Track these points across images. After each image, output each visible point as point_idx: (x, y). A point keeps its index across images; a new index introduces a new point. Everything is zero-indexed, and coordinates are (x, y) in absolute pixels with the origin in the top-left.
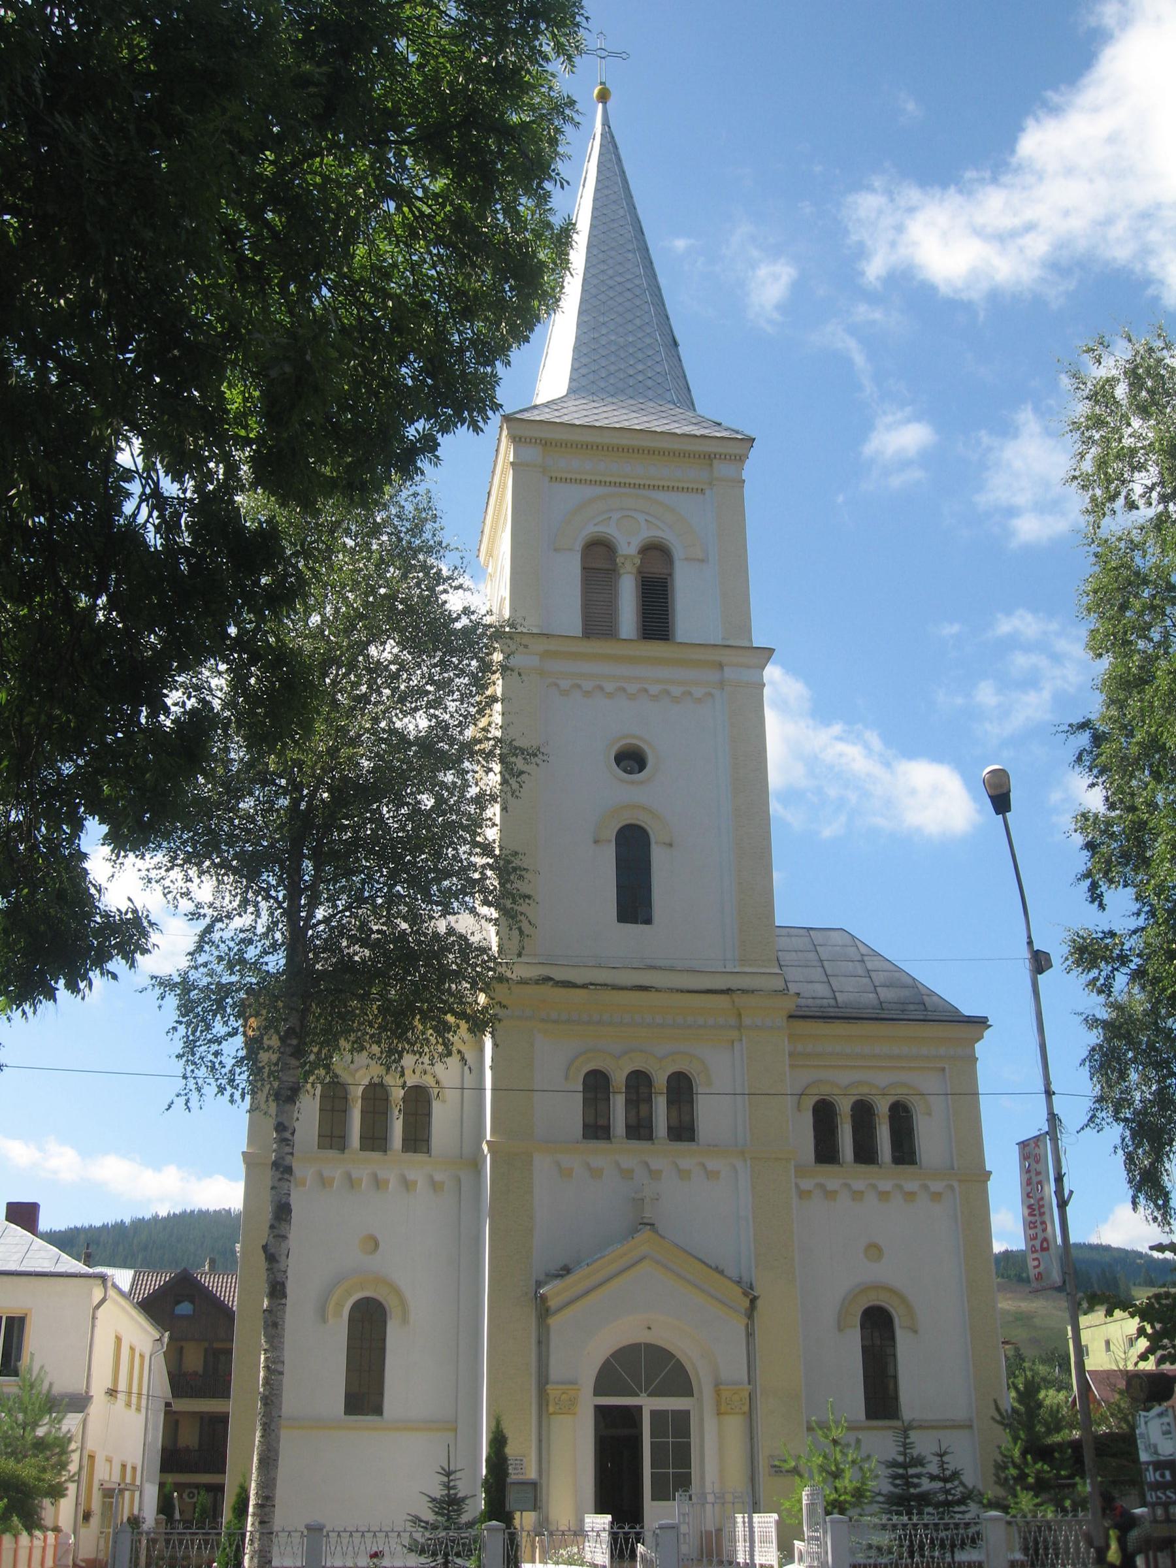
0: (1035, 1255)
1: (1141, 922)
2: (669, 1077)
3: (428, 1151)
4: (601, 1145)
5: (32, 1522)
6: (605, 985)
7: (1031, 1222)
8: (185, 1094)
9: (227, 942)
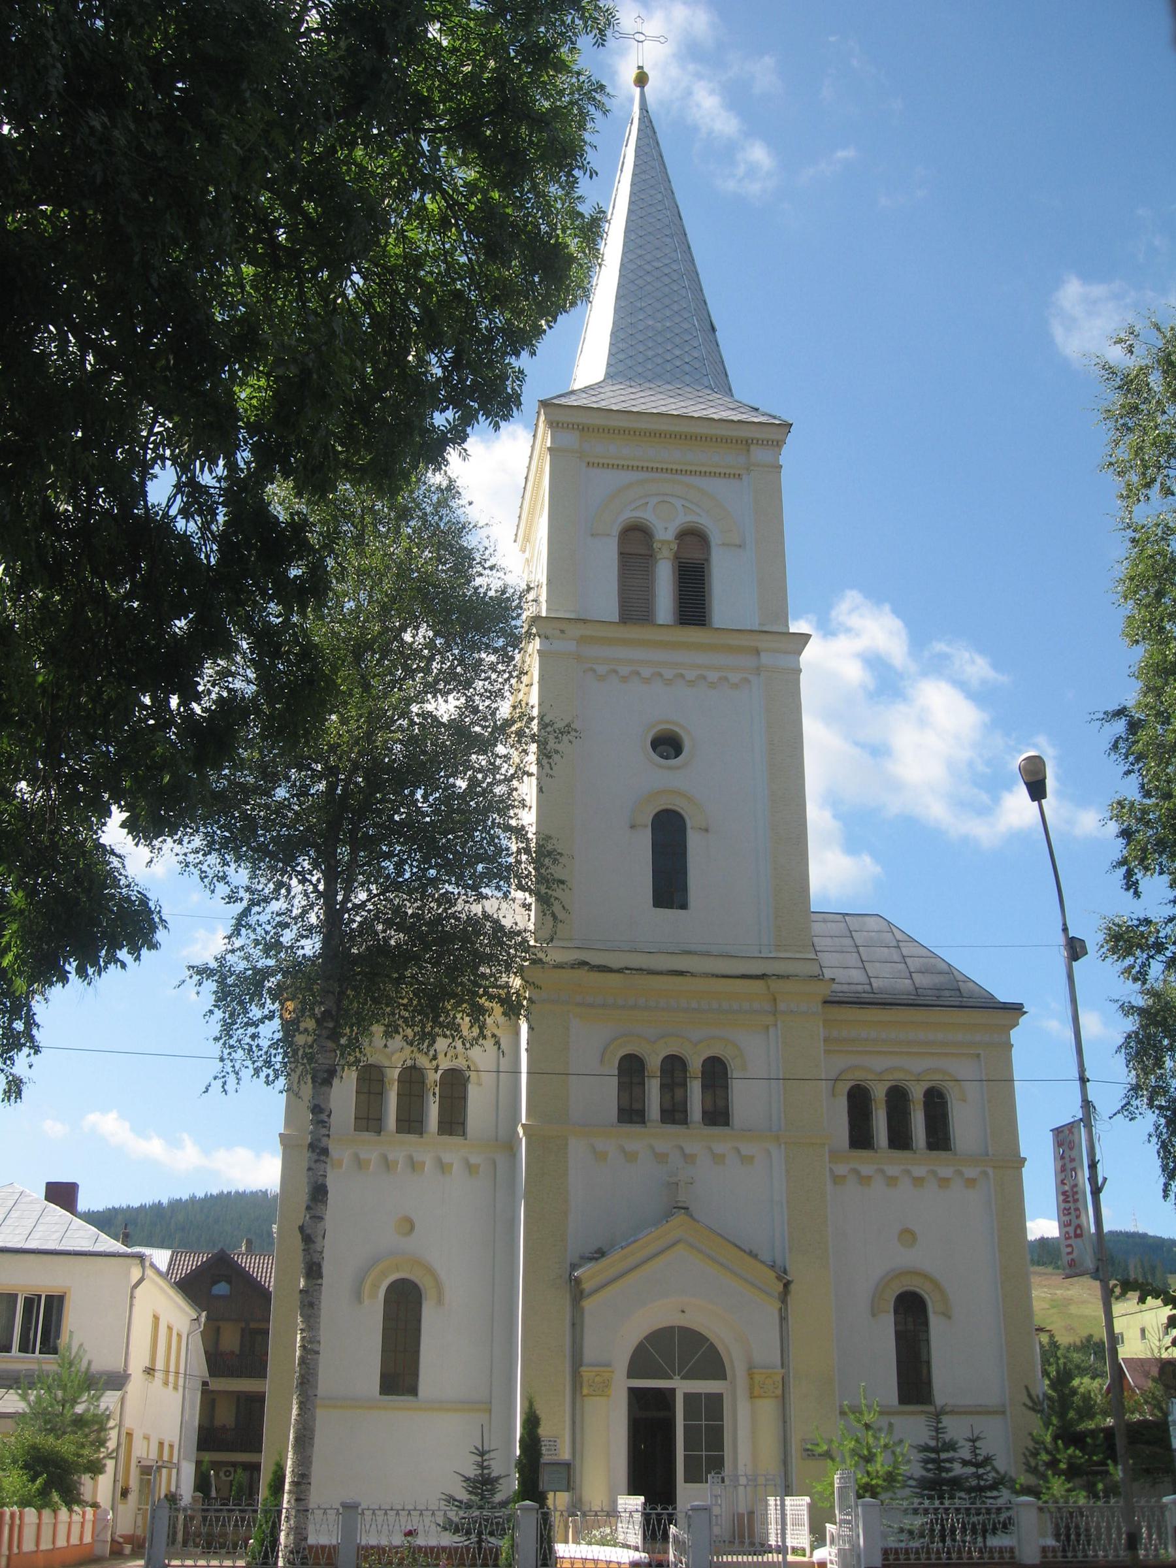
0: (1069, 1242)
3: (464, 1134)
4: (636, 1129)
5: (71, 1497)
6: (641, 970)
8: (222, 1077)
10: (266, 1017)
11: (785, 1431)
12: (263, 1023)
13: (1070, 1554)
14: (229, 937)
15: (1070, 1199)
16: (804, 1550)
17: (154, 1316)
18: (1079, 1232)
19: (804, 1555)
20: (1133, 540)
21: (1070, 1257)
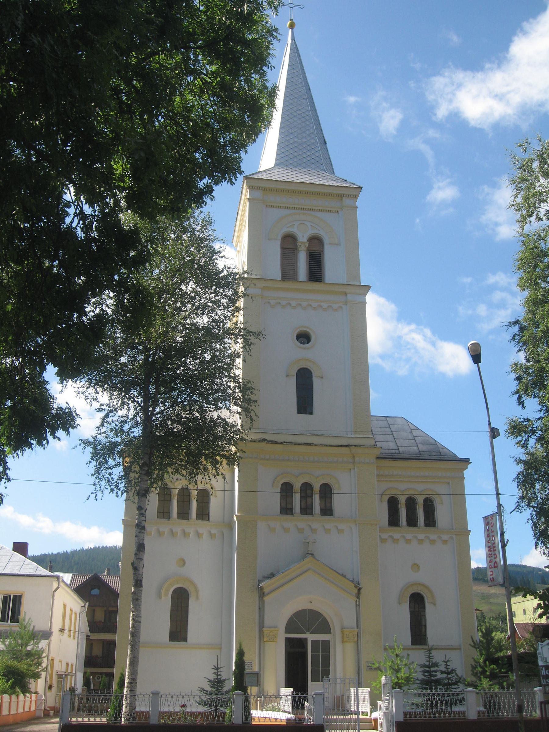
1: (542, 414)
2: (321, 485)
3: (208, 520)
4: (289, 517)
5: (25, 690)
6: (291, 443)
7: (489, 554)
8: (95, 493)
9: (115, 422)
13: (491, 715)
14: (99, 427)
16: (367, 713)
17: (64, 605)
18: (496, 565)
20: (523, 242)
21: (492, 576)
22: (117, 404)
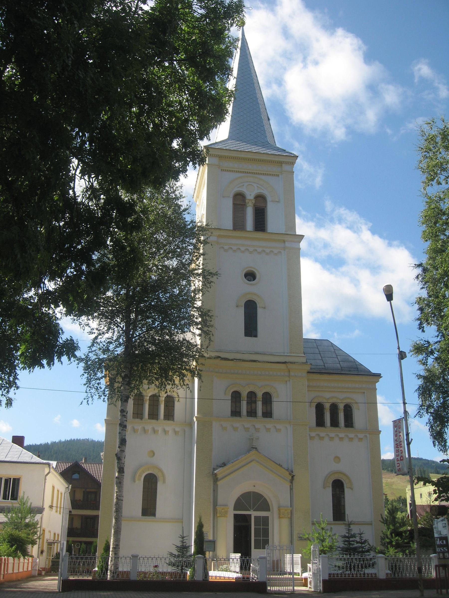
0: (398, 462)
1: (439, 339)
2: (263, 394)
3: (173, 420)
4: (238, 419)
5: (25, 553)
6: (240, 360)
7: (397, 450)
8: (87, 399)
9: (103, 343)
10: (103, 377)
11: (291, 530)
12: (102, 379)
13: (396, 575)
14: (90, 347)
15: (399, 446)
18: (402, 458)
19: (299, 575)
21: (399, 468)
22: (104, 328)
